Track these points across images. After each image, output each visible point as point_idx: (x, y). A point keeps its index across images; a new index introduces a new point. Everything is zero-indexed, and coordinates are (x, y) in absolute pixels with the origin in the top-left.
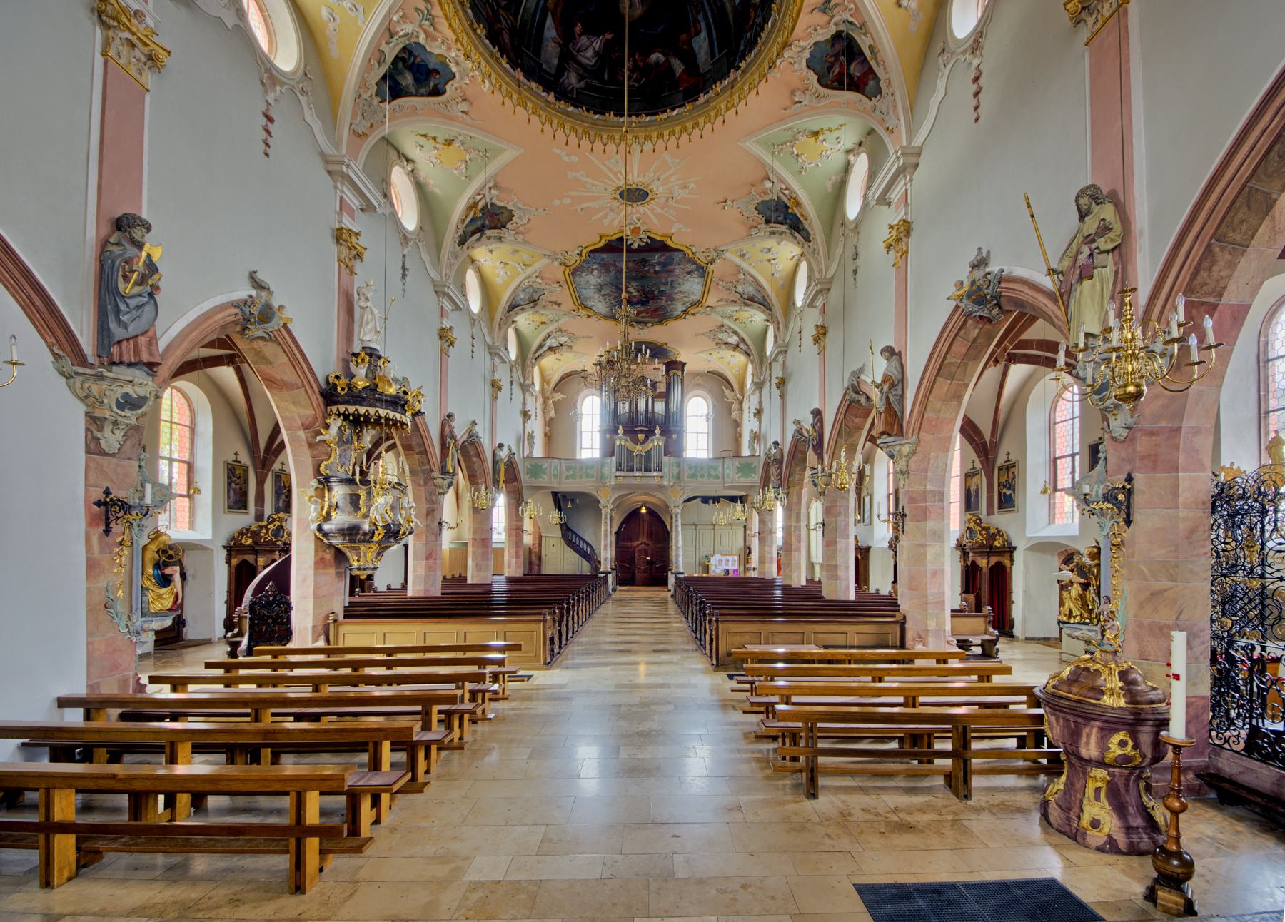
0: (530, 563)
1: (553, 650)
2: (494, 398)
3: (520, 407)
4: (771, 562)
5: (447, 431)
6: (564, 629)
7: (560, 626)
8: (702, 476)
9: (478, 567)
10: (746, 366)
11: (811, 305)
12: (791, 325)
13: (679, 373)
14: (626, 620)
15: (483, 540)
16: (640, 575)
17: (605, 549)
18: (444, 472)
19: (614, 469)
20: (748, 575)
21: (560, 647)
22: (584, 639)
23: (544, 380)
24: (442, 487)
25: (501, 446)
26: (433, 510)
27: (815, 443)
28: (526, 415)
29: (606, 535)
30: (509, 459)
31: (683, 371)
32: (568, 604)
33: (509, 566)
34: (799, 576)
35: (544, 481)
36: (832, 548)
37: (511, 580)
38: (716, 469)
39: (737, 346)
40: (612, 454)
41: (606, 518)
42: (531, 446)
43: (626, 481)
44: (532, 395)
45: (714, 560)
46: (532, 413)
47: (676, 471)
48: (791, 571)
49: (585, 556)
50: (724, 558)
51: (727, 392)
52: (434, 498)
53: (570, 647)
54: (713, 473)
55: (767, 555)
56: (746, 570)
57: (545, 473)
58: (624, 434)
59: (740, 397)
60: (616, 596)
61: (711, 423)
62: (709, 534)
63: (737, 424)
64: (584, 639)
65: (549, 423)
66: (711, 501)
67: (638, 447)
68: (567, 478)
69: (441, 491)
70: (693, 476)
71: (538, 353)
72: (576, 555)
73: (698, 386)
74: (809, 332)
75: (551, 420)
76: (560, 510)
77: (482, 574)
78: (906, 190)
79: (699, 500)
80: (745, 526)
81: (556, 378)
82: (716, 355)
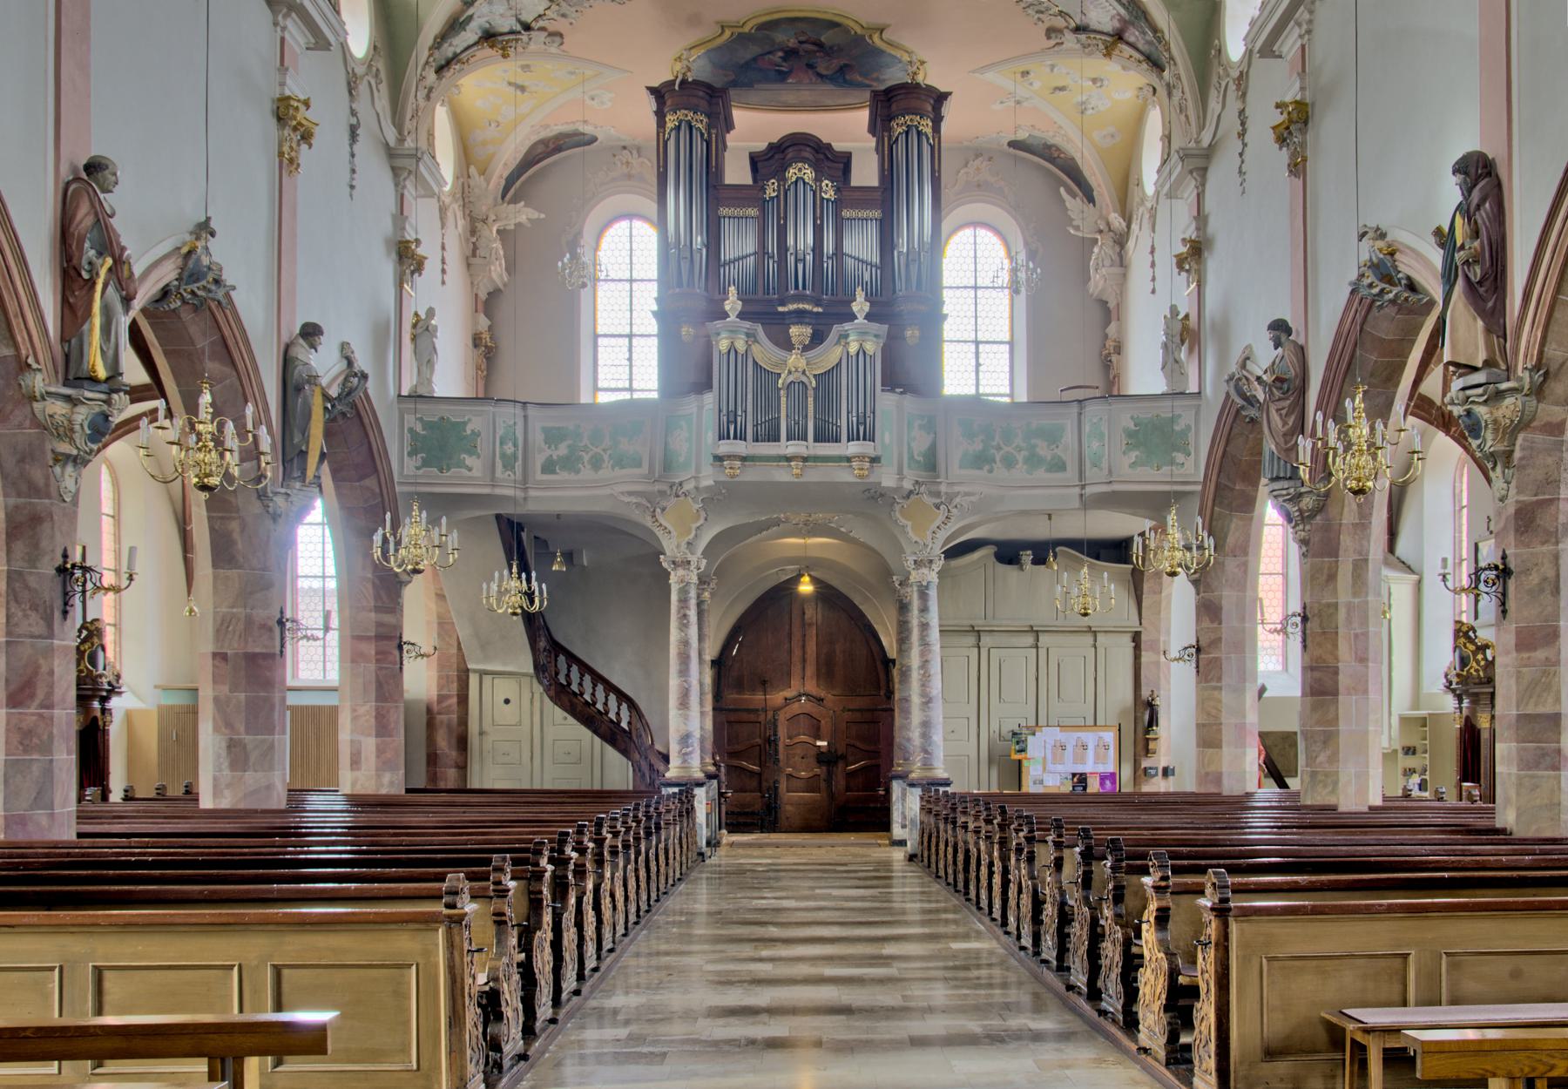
0: (433, 759)
1: (495, 1045)
2: (287, 163)
3: (387, 225)
4: (1241, 743)
5: (83, 217)
6: (543, 960)
7: (526, 945)
8: (1009, 463)
9: (237, 755)
10: (1139, 120)
11: (1268, 50)
12: (1214, 105)
13: (926, 126)
14: (774, 931)
15: (252, 659)
16: (793, 798)
17: (684, 703)
18: (74, 374)
19: (710, 435)
20: (1147, 788)
21: (529, 1032)
22: (618, 1000)
23: (466, 153)
24: (67, 433)
25: (311, 333)
26: (36, 520)
27: (1477, 272)
28: (407, 257)
29: (684, 659)
30: (347, 393)
31: (937, 121)
32: (560, 861)
33: (355, 763)
34: (1363, 777)
35: (470, 475)
36: (1540, 654)
37: (359, 803)
38: (1053, 437)
39: (1119, 36)
40: (705, 385)
41: (683, 601)
42: (426, 359)
43: (752, 475)
44: (430, 194)
45: (1036, 747)
46: (428, 250)
47: (921, 444)
48: (1334, 758)
49: (613, 735)
50: (1071, 738)
51: (1074, 205)
52: (37, 474)
53: (570, 1031)
54: (1043, 450)
55: (1227, 720)
56: (1141, 774)
57: (472, 451)
58: (742, 316)
59: (1117, 221)
60: (718, 858)
61: (1022, 299)
62: (1016, 662)
63: (1108, 312)
64: (618, 1000)
65: (488, 303)
66: (1027, 557)
67: (795, 360)
68: (549, 467)
69: (65, 448)
70: (981, 460)
71: (448, 50)
72: (585, 733)
73: (979, 189)
74: (1264, 119)
75: (495, 294)
76: (524, 568)
77: (250, 777)
78: (1303, 47)
79: (987, 551)
80: (1136, 638)
81: (509, 154)
82: (1042, 78)
